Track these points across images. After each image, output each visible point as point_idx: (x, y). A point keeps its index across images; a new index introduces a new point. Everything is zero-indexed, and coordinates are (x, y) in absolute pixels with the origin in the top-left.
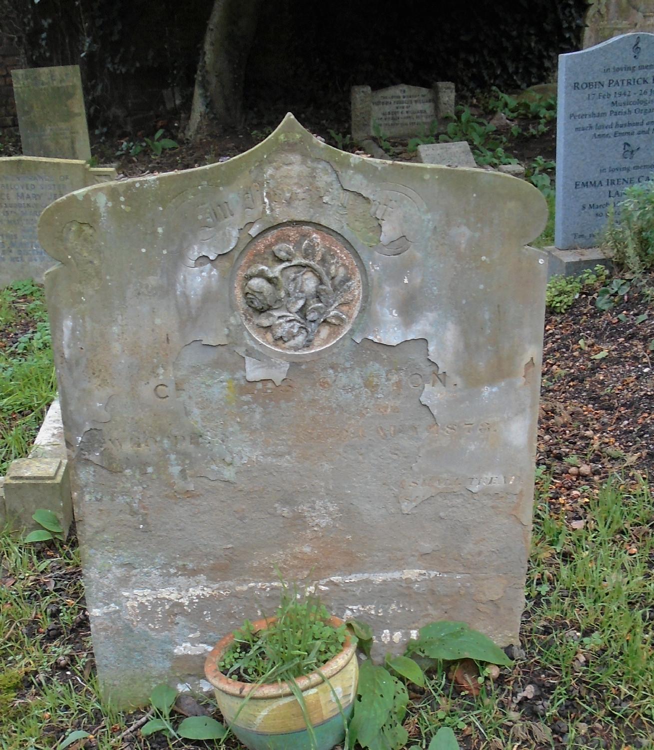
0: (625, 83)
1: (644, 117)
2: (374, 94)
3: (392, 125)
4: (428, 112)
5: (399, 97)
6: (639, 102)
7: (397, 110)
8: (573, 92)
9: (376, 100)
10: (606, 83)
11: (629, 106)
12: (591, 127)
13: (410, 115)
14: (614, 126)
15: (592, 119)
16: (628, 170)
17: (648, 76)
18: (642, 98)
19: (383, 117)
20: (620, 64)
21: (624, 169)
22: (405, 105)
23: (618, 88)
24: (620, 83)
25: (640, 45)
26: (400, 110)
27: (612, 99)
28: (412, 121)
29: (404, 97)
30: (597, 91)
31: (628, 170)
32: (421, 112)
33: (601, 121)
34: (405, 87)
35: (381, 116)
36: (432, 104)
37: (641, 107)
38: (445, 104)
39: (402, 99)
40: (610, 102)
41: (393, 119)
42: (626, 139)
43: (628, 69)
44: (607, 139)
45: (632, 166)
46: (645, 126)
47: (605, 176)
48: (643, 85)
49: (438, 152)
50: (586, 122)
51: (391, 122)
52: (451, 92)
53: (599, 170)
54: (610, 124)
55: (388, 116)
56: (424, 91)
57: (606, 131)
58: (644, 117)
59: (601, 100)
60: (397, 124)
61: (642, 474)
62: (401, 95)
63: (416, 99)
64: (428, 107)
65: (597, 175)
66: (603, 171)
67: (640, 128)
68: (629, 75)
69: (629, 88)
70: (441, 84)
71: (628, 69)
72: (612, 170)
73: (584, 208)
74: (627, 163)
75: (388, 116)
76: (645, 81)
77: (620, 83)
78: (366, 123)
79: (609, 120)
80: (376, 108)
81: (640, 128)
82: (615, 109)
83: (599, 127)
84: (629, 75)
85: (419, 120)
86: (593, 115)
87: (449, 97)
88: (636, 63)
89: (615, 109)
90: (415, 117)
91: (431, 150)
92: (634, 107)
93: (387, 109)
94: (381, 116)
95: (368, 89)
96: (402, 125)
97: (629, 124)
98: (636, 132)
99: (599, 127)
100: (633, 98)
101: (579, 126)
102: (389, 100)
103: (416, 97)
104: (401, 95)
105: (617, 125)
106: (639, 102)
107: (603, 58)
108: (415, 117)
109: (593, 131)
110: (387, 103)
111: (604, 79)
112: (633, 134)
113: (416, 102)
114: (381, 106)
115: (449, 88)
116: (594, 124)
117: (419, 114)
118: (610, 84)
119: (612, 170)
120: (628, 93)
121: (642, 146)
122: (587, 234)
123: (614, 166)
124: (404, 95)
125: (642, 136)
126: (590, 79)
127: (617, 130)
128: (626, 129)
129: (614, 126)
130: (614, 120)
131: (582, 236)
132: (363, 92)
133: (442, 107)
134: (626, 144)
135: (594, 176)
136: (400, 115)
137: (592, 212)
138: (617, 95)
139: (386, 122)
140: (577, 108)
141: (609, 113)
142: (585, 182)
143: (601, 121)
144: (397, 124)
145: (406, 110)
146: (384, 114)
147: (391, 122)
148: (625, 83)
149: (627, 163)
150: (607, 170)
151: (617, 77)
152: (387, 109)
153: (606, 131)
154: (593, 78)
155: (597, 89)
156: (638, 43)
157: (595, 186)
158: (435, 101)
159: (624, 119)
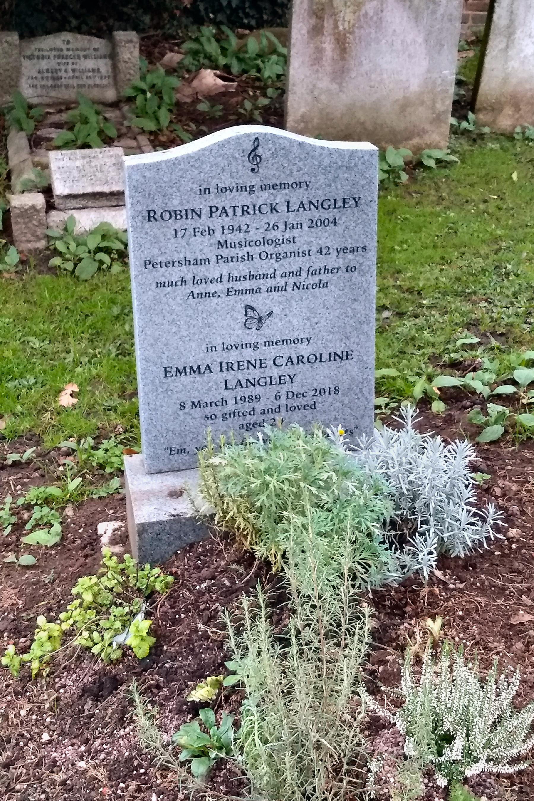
0: (239, 211)
1: (276, 266)
2: (24, 44)
3: (51, 86)
4: (103, 70)
5: (61, 50)
6: (265, 242)
7: (58, 67)
8: (147, 225)
9: (29, 53)
10: (205, 212)
11: (248, 249)
12: (183, 281)
13: (77, 74)
14: (225, 279)
15: (184, 268)
16: (255, 347)
17: (278, 201)
18: (270, 235)
19: (39, 76)
20: (227, 181)
21: (248, 345)
22: (70, 61)
23: (226, 219)
24: (230, 212)
25: (260, 151)
26: (63, 68)
27: (218, 236)
28: (81, 82)
29: (68, 50)
30: (190, 223)
31: (255, 347)
32: (94, 70)
33: (202, 271)
34: (67, 36)
35: (36, 74)
36: (109, 62)
37: (270, 249)
38: (126, 62)
39: (65, 53)
40: (214, 241)
41: (53, 78)
42: (248, 299)
43: (241, 189)
44: (215, 300)
45: (261, 341)
46: (278, 278)
47: (219, 356)
48: (271, 216)
49: (78, 163)
50: (175, 274)
51: (50, 83)
52: (134, 47)
53: (204, 347)
54: (217, 276)
55: (45, 75)
56: (97, 43)
57: (212, 288)
58: (276, 266)
59: (199, 238)
60: (60, 86)
61: (403, 665)
62: (64, 47)
63: (85, 53)
64: (104, 66)
65: (202, 355)
66: (211, 349)
67: (270, 283)
68: (244, 199)
69: (246, 219)
70: (120, 35)
71: (241, 189)
72: (227, 348)
73: (183, 406)
74: (252, 336)
75: (45, 75)
76: (273, 209)
77: (230, 212)
78: (12, 83)
79: (214, 271)
80: (26, 63)
81: (270, 283)
82: (225, 252)
83: (195, 282)
84: (244, 199)
85: (90, 82)
86: (187, 262)
87: (131, 53)
88: (255, 181)
89: (225, 252)
90: (84, 77)
91: (66, 159)
92: (255, 251)
93: (44, 64)
94: (36, 74)
95: (14, 37)
96: (67, 87)
97: (251, 277)
98: (264, 289)
99: (195, 282)
100: (254, 235)
101: (162, 280)
102: (46, 53)
103: (85, 50)
104: (64, 47)
105: (230, 278)
106: (265, 242)
107: (197, 172)
108: (84, 77)
109: (189, 288)
110: (43, 57)
111: (202, 204)
112: (259, 291)
113: (86, 57)
114: (35, 61)
115: (131, 41)
116: (189, 277)
117: (90, 74)
118: (211, 212)
119: (227, 348)
120: (244, 228)
121: (276, 310)
122: (191, 448)
123: (229, 341)
124: (68, 46)
125: (275, 295)
126: (175, 204)
127: (230, 286)
128: (247, 285)
129: (225, 279)
130: (224, 269)
131: (183, 451)
132: (7, 42)
133: (122, 66)
134: (248, 307)
135: (195, 356)
136: (63, 74)
137: (198, 412)
138: (226, 231)
139: (43, 83)
140: (156, 251)
141: (214, 259)
142: (181, 368)
143: (202, 271)
144: (60, 86)
145: (70, 67)
146: (39, 72)
147: (50, 83)
148: (239, 211)
149: (252, 336)
150: (219, 348)
151: (222, 201)
152: (44, 64)
153: (212, 288)
154: (182, 203)
155: (189, 221)
156: (255, 149)
157: (199, 372)
158: (113, 56)
159: (243, 269)
